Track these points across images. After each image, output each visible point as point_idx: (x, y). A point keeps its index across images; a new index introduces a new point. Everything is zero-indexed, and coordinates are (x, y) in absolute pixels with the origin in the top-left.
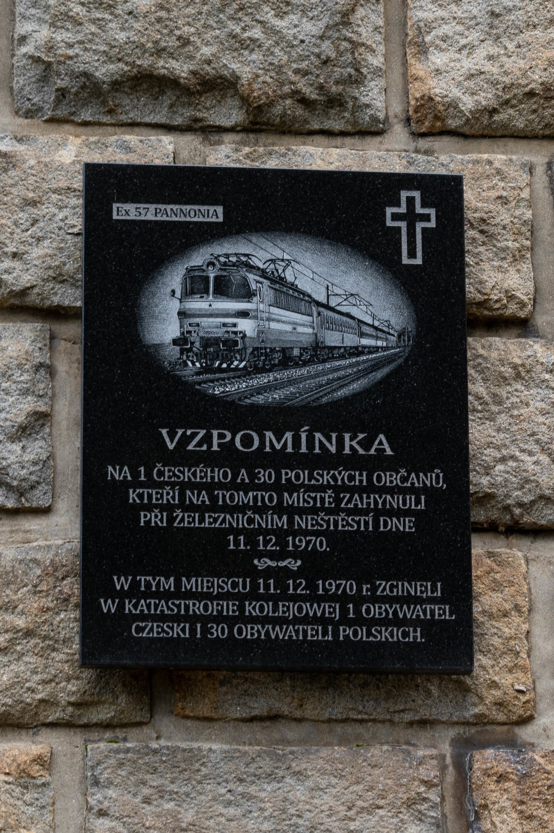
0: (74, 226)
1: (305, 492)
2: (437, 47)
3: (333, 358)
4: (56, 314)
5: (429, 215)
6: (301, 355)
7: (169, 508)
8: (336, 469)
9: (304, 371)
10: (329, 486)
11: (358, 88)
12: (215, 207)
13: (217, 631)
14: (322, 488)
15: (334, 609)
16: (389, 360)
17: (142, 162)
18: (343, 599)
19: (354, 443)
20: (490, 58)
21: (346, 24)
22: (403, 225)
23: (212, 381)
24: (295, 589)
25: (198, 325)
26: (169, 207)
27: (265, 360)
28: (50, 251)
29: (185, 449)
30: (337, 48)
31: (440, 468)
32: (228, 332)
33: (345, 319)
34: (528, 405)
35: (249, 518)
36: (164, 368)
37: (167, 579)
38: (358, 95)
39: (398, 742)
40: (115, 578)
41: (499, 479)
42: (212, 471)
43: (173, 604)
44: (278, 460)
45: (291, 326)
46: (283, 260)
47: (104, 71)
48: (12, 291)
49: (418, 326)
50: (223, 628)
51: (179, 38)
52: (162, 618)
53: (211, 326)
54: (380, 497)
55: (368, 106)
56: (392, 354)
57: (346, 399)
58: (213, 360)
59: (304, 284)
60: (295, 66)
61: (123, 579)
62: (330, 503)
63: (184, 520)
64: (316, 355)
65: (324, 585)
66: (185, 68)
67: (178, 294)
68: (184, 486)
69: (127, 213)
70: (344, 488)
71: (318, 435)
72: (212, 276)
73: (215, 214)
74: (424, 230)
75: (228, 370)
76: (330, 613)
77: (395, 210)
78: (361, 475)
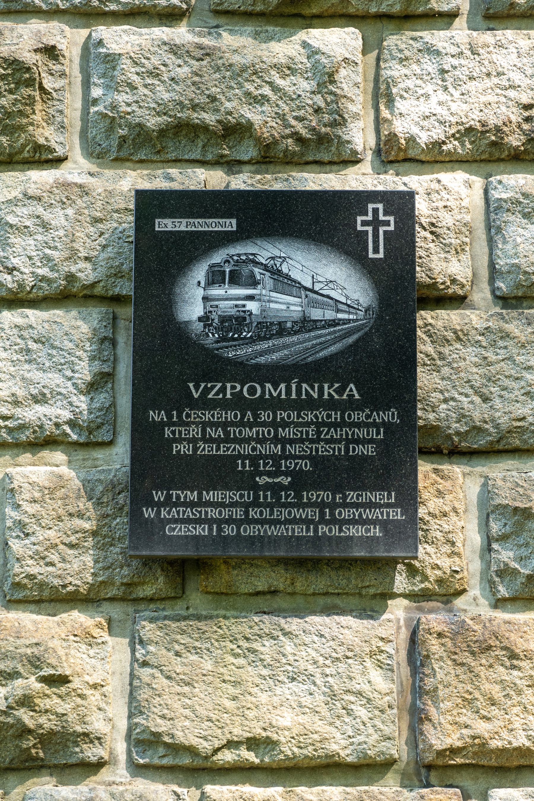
0: (129, 236)
1: (294, 427)
2: (401, 97)
3: (317, 328)
4: (118, 300)
5: (389, 221)
6: (293, 326)
7: (193, 441)
8: (317, 410)
9: (295, 338)
10: (312, 423)
11: (341, 129)
12: (231, 220)
13: (229, 531)
14: (308, 424)
15: (315, 512)
16: (358, 329)
17: (181, 188)
18: (322, 505)
19: (331, 391)
20: (440, 103)
21: (333, 82)
22: (370, 229)
23: (227, 347)
24: (286, 498)
25: (217, 306)
26: (196, 221)
27: (266, 331)
28: (112, 255)
29: (206, 397)
30: (325, 100)
31: (396, 408)
32: (239, 311)
33: (325, 299)
34: (465, 359)
35: (253, 447)
36: (192, 339)
37: (192, 492)
38: (341, 134)
39: (365, 610)
40: (154, 492)
41: (443, 415)
42: (226, 413)
43: (196, 510)
44: (276, 404)
45: (286, 306)
46: (280, 257)
47: (153, 122)
48: (84, 285)
49: (380, 303)
50: (233, 528)
51: (209, 96)
52: (188, 521)
53: (226, 307)
54: (350, 430)
55: (348, 142)
56: (361, 325)
57: (326, 359)
58: (228, 332)
59: (295, 275)
60: (294, 114)
61: (160, 493)
62: (313, 435)
63: (204, 449)
64: (304, 327)
65: (307, 495)
66: (213, 118)
67: (203, 284)
68: (205, 425)
69: (166, 226)
70: (324, 424)
71: (304, 385)
72: (228, 270)
73: (230, 225)
74: (385, 232)
75: (239, 338)
76: (312, 516)
77: (364, 218)
78: (336, 414)
